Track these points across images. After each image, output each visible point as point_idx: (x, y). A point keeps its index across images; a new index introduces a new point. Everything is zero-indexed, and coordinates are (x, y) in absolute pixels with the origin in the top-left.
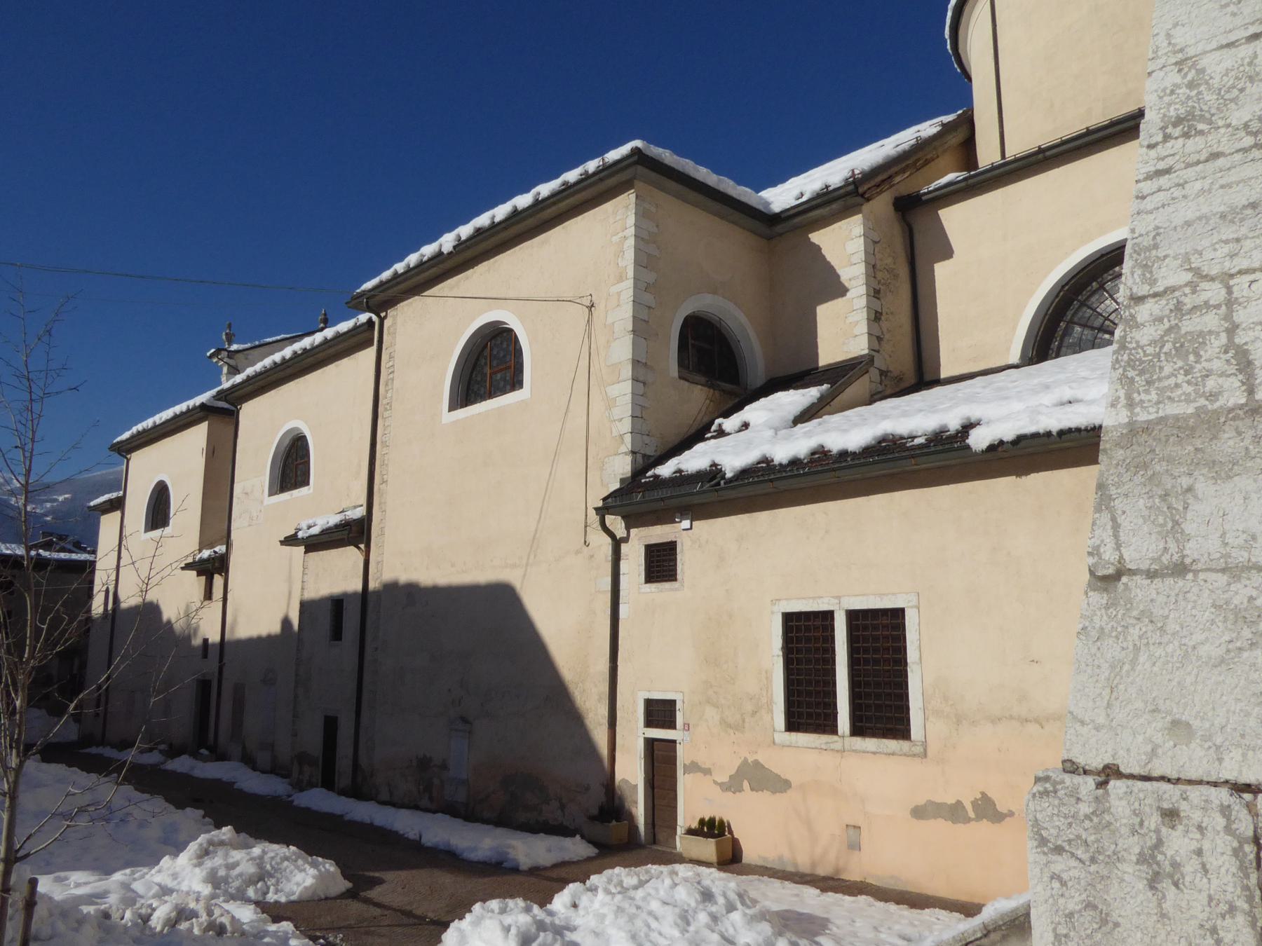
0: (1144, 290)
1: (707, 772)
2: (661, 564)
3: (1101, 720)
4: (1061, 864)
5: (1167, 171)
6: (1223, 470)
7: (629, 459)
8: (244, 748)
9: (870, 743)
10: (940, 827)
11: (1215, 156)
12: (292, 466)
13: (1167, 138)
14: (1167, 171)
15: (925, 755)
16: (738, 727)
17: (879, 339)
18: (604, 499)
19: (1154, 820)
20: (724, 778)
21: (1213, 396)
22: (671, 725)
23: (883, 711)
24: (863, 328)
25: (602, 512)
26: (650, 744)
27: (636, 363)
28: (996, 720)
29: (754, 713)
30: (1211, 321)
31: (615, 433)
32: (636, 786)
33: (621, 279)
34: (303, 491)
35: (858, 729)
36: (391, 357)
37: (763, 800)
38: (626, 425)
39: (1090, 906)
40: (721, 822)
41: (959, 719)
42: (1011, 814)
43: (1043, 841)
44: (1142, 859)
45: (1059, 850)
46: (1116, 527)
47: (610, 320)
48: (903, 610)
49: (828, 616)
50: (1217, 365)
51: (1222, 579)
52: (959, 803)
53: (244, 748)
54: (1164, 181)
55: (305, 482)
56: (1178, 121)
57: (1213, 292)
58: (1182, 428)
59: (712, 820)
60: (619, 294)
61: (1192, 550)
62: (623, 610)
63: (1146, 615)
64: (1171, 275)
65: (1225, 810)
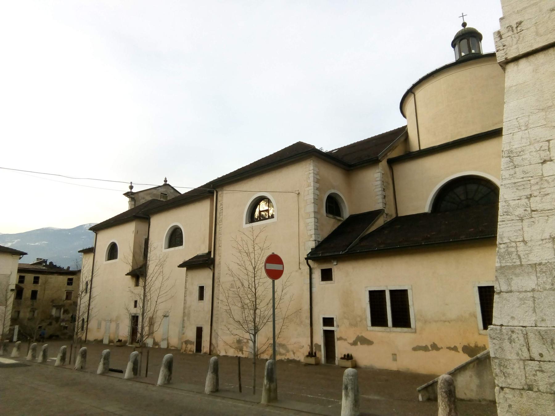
0: (501, 242)
1: (345, 340)
2: (327, 276)
3: (499, 317)
4: (494, 341)
5: (504, 221)
6: (517, 275)
7: (314, 242)
8: (154, 340)
9: (399, 329)
10: (421, 353)
11: (513, 220)
12: (175, 238)
13: (504, 215)
14: (504, 221)
15: (415, 332)
16: (355, 325)
17: (385, 204)
18: (307, 255)
19: (510, 333)
20: (351, 341)
21: (515, 262)
22: (332, 325)
23: (402, 319)
24: (381, 200)
25: (307, 259)
26: (325, 332)
27: (315, 212)
28: (436, 322)
29: (360, 321)
30: (513, 249)
31: (309, 234)
32: (320, 346)
33: (309, 186)
34: (180, 247)
35: (395, 325)
36: (221, 204)
37: (365, 347)
38: (313, 232)
39: (500, 347)
40: (351, 356)
41: (426, 322)
42: (442, 348)
43: (491, 338)
44: (508, 339)
45: (494, 339)
46: (499, 284)
47: (305, 199)
48: (407, 290)
49: (383, 292)
50: (515, 257)
51: (518, 293)
52: (426, 346)
53: (154, 340)
54: (504, 223)
55: (181, 243)
56: (506, 212)
57: (514, 244)
58: (509, 268)
59: (348, 355)
60: (308, 191)
61: (513, 289)
62: (314, 290)
63: (506, 299)
64: (506, 240)
65: (522, 330)
